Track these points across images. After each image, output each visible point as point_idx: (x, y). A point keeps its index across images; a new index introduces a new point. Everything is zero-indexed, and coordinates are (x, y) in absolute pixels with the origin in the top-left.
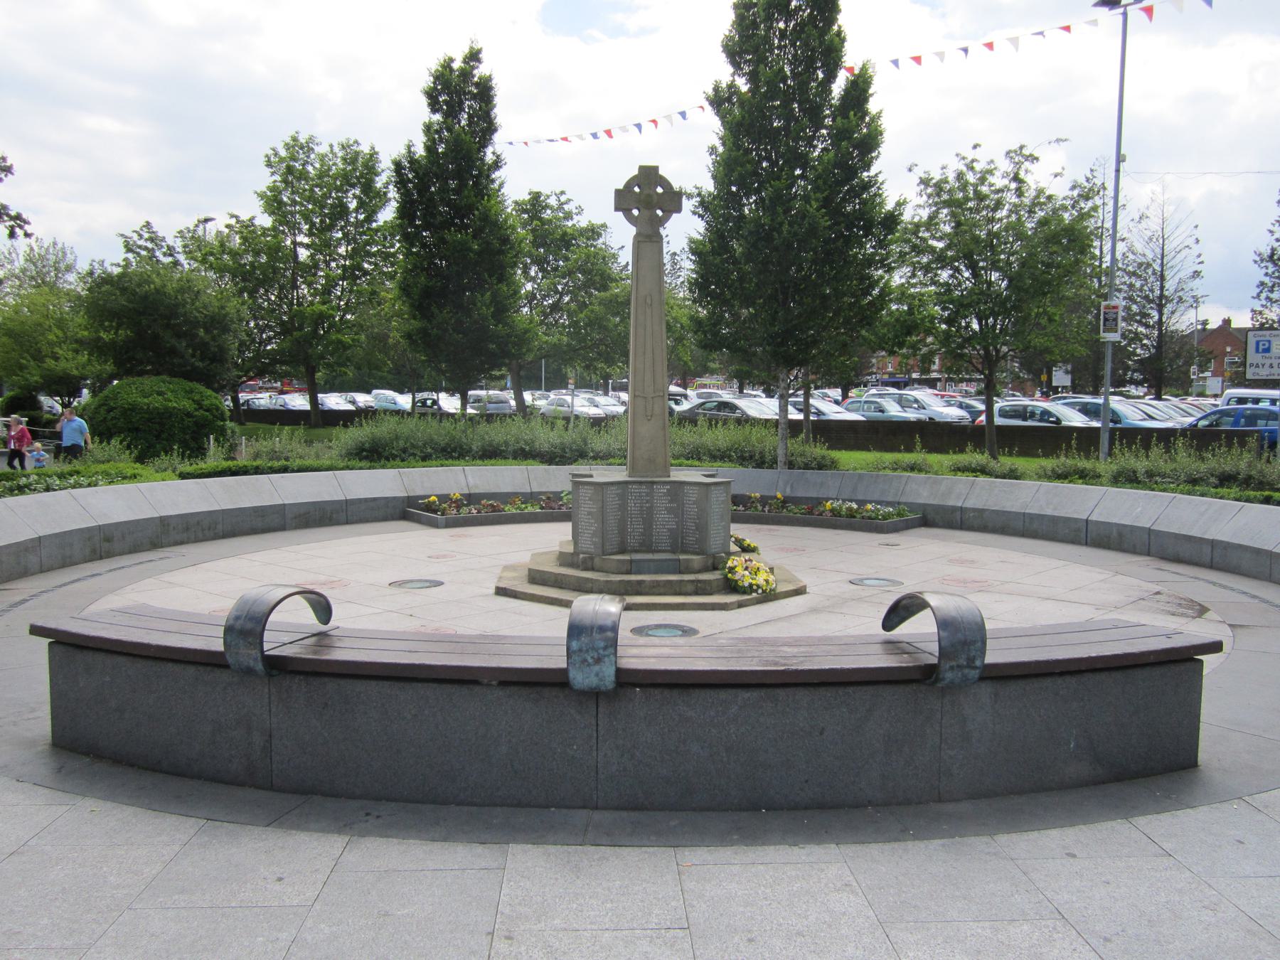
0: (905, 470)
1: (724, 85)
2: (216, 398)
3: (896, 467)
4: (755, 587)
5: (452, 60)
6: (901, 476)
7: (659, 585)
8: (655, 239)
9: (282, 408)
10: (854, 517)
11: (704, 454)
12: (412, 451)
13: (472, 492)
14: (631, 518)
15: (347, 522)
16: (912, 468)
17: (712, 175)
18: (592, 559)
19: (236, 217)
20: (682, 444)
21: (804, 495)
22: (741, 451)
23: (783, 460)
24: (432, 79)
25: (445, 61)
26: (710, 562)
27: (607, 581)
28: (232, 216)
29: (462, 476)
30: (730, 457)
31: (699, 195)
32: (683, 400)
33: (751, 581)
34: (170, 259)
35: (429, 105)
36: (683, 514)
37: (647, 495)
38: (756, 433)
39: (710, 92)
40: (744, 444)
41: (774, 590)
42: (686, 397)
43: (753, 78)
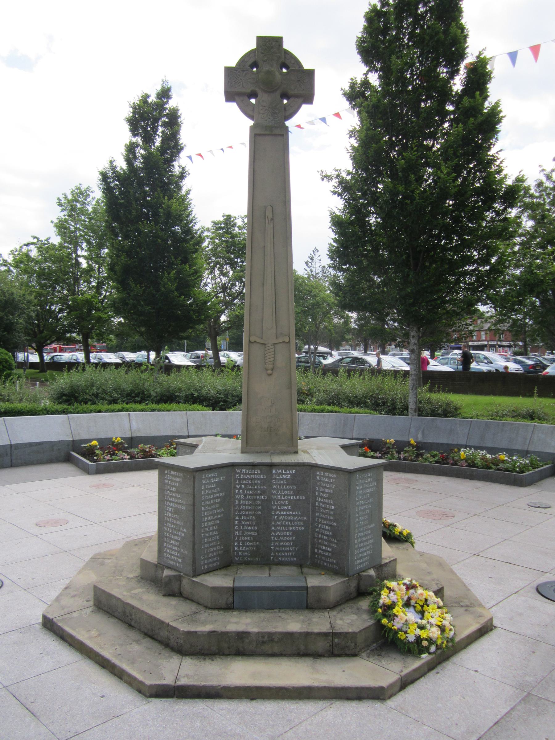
0: (524, 417)
1: (359, 82)
2: (6, 354)
3: (517, 415)
4: (425, 643)
5: (148, 96)
6: (528, 425)
7: (272, 640)
8: (277, 132)
9: (75, 361)
10: (490, 468)
11: (344, 400)
12: (103, 396)
13: (134, 435)
14: (240, 516)
15: (12, 466)
16: (532, 416)
17: (351, 156)
18: (179, 578)
19: (38, 238)
20: (325, 391)
21: (435, 441)
22: (375, 398)
23: (414, 407)
24: (131, 110)
25: (142, 97)
26: (353, 585)
27: (189, 633)
28: (35, 238)
29: (126, 421)
30: (365, 403)
31: (338, 176)
32: (329, 356)
33: (418, 632)
34: (6, 268)
35: (131, 130)
36: (314, 511)
37: (263, 484)
38: (388, 384)
39: (347, 88)
40: (378, 391)
41: (452, 640)
42: (331, 355)
43: (385, 79)
